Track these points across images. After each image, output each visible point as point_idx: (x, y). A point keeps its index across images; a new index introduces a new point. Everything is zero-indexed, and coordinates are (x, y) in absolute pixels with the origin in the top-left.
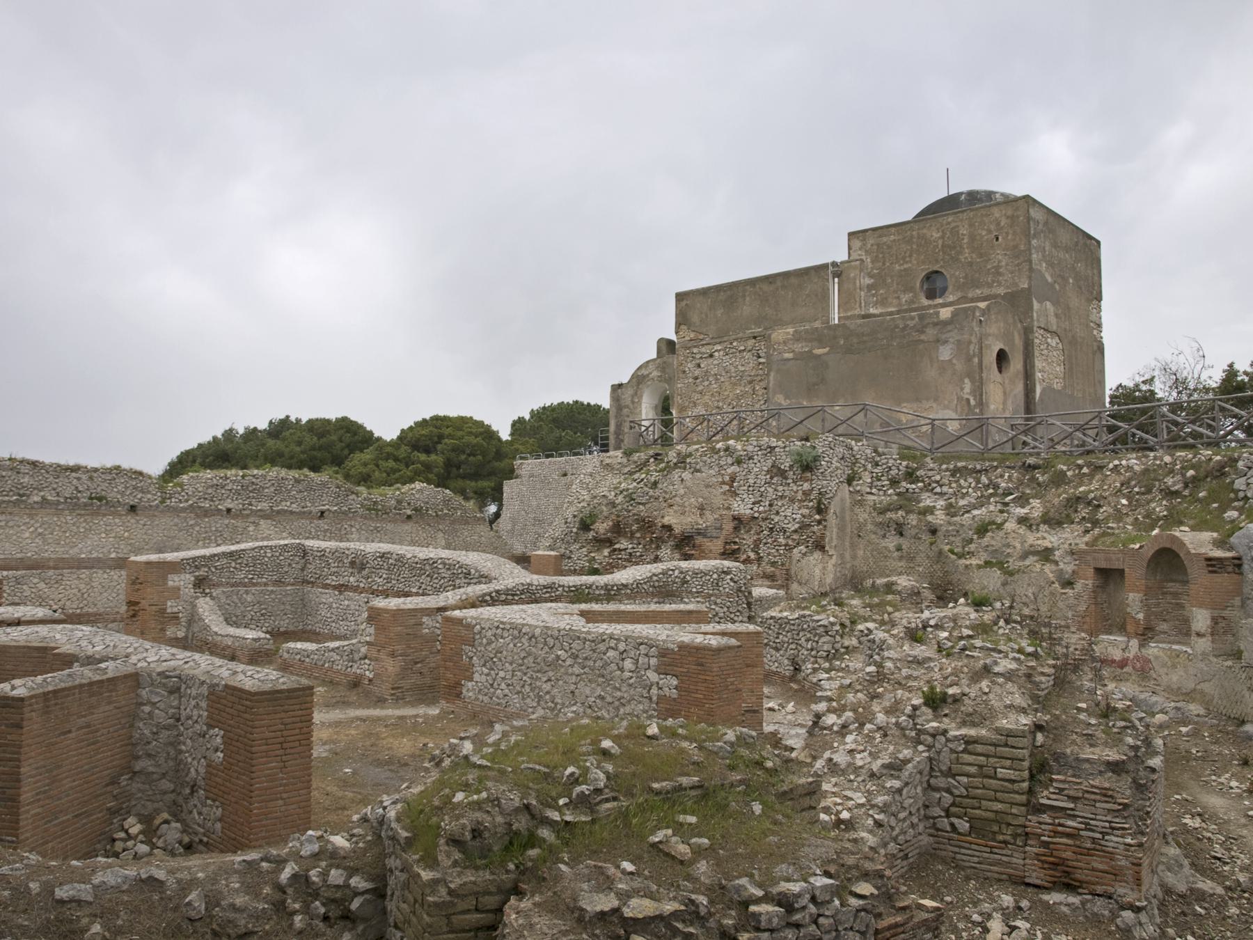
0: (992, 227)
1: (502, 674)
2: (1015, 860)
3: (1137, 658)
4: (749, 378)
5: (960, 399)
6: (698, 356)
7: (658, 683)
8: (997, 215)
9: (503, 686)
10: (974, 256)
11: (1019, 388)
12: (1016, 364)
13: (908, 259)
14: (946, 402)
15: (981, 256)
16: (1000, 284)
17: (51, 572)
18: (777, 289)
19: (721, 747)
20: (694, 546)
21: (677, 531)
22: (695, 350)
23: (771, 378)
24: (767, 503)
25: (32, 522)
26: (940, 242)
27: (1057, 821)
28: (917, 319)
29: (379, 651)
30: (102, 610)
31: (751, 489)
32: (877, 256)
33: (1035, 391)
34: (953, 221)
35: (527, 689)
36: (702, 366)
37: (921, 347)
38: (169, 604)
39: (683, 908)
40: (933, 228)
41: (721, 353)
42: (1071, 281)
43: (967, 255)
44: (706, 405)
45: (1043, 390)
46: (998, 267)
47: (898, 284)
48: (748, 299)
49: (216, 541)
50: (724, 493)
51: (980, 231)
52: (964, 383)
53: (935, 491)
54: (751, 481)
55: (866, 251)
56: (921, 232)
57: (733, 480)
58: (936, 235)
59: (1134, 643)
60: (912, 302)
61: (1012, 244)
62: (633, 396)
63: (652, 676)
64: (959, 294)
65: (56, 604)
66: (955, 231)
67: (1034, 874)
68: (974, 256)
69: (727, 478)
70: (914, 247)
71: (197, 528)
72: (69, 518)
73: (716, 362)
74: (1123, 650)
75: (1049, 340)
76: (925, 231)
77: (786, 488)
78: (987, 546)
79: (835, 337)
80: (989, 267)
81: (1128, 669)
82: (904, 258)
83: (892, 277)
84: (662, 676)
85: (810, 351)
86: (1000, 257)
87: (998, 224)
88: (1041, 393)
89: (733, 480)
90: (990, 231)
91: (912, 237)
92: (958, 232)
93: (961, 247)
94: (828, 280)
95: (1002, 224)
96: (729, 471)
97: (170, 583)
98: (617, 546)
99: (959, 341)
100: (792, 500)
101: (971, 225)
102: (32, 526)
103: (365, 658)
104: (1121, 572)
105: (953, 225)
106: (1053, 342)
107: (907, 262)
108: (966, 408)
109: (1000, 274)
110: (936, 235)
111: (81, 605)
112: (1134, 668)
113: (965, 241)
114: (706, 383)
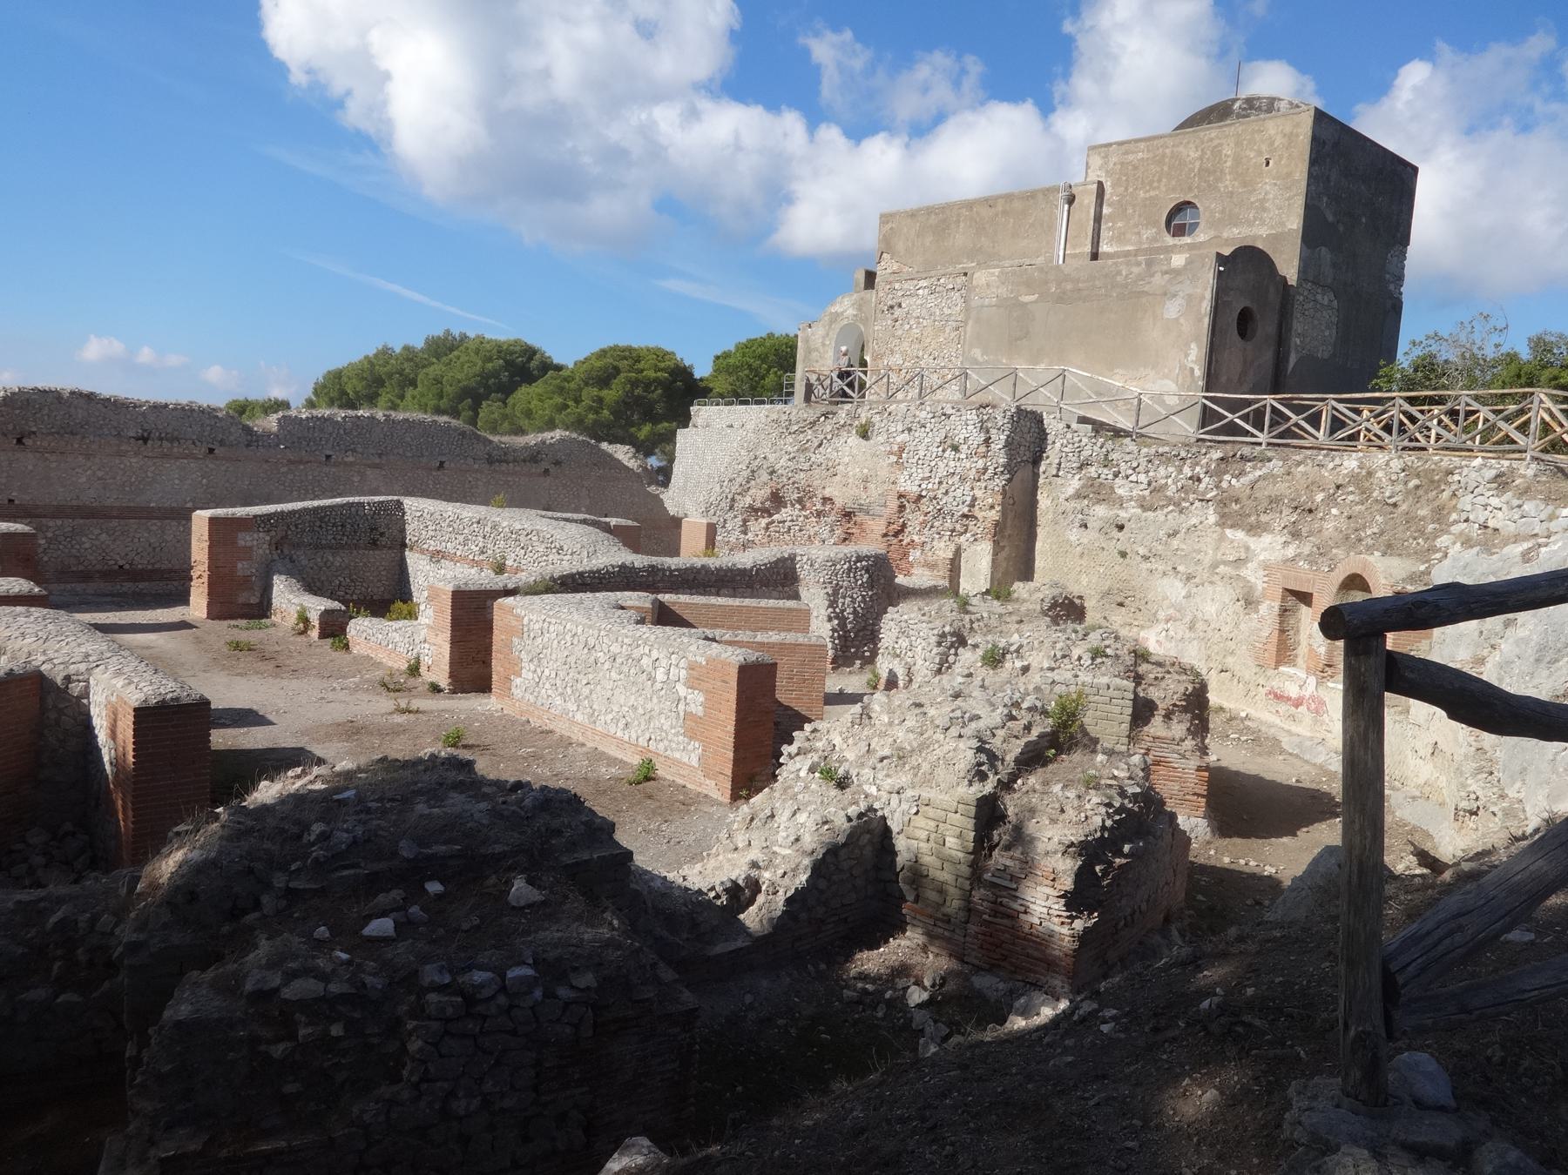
0: (1264, 148)
1: (547, 672)
2: (956, 937)
3: (1312, 697)
4: (954, 324)
5: (1182, 367)
6: (900, 293)
7: (685, 698)
8: (1272, 132)
9: (547, 686)
10: (1236, 184)
11: (1268, 356)
12: (1266, 327)
13: (1155, 184)
14: (1166, 371)
15: (1245, 184)
16: (1263, 223)
17: (115, 523)
18: (997, 215)
19: (514, 812)
20: (855, 524)
21: (839, 503)
22: (897, 286)
23: (969, 328)
24: (937, 480)
25: (89, 464)
26: (1197, 164)
27: (999, 900)
28: (1143, 266)
29: (437, 635)
30: (177, 567)
31: (920, 462)
32: (1119, 179)
33: (1287, 361)
34: (1217, 137)
35: (569, 690)
36: (903, 305)
37: (1144, 300)
38: (240, 565)
39: (353, 991)
40: (1191, 145)
41: (926, 290)
42: (1364, 220)
43: (1228, 183)
44: (904, 354)
45: (1300, 361)
46: (1263, 201)
47: (1140, 216)
48: (962, 225)
49: (314, 492)
50: (891, 465)
51: (1248, 153)
52: (1190, 349)
53: (1130, 479)
54: (921, 453)
55: (1107, 172)
56: (1175, 149)
57: (902, 450)
58: (1194, 154)
59: (1312, 680)
60: (1154, 239)
61: (1285, 170)
62: (824, 338)
63: (682, 690)
64: (1212, 233)
65: (122, 559)
66: (1217, 151)
67: (974, 953)
68: (1236, 184)
69: (896, 448)
70: (1166, 168)
71: (290, 477)
72: (135, 460)
73: (919, 302)
74: (1301, 687)
75: (1319, 297)
76: (1181, 149)
77: (958, 464)
78: (1177, 550)
79: (1046, 282)
80: (1252, 200)
81: (1303, 709)
82: (1151, 185)
83: (1134, 206)
84: (690, 691)
85: (1016, 298)
86: (1268, 187)
87: (1272, 143)
88: (1296, 364)
89: (902, 450)
90: (1260, 153)
91: (1164, 155)
92: (1220, 151)
93: (1222, 171)
94: (1057, 206)
95: (1276, 144)
96: (899, 439)
97: (241, 543)
98: (776, 517)
99: (1190, 296)
100: (963, 480)
101: (1238, 144)
102: (90, 468)
103: (425, 641)
104: (891, 670)
105: (1216, 142)
106: (1325, 298)
107: (1154, 189)
108: (1189, 379)
109: (1264, 209)
110: (1194, 154)
111: (153, 561)
112: (1308, 709)
113: (1228, 164)
114: (907, 327)
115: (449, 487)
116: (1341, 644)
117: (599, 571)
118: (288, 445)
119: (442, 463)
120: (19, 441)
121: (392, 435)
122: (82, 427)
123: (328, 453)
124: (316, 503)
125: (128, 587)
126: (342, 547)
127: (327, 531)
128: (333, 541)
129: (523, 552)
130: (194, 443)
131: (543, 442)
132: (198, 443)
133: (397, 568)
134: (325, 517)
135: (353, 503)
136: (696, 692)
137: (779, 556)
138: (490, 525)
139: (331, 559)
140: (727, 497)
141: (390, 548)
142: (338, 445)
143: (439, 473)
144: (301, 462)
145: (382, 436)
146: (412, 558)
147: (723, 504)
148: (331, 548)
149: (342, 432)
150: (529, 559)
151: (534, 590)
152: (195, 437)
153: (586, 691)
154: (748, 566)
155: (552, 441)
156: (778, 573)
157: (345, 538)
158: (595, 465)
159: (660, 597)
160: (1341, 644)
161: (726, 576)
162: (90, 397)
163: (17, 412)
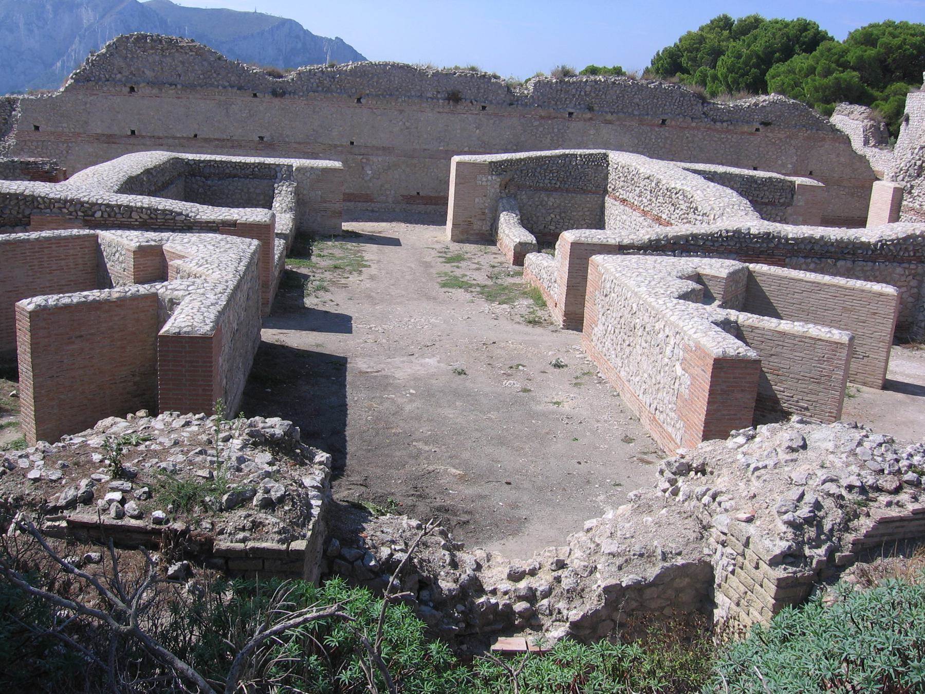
115: (668, 142)
116: (499, 638)
117: (712, 235)
118: (540, 103)
119: (664, 121)
120: (359, 100)
121: (623, 96)
122: (397, 90)
123: (571, 110)
124: (539, 153)
125: (421, 208)
126: (556, 190)
127: (545, 176)
128: (549, 185)
129: (673, 208)
130: (471, 102)
131: (756, 105)
132: (475, 103)
133: (598, 210)
134: (544, 165)
135: (568, 154)
136: (687, 375)
137: (909, 232)
138: (655, 182)
139: (546, 199)
140: (915, 165)
141: (594, 193)
142: (579, 104)
143: (662, 129)
144: (549, 118)
145: (615, 97)
146: (609, 201)
147: (911, 171)
148: (547, 190)
149: (583, 93)
150: (676, 215)
151: (622, 249)
152: (472, 98)
153: (627, 350)
154: (873, 241)
155: (764, 104)
156: (906, 250)
157: (559, 184)
158: (804, 126)
159: (752, 266)
160: (499, 638)
161: (847, 248)
162: (406, 68)
163: (358, 80)
